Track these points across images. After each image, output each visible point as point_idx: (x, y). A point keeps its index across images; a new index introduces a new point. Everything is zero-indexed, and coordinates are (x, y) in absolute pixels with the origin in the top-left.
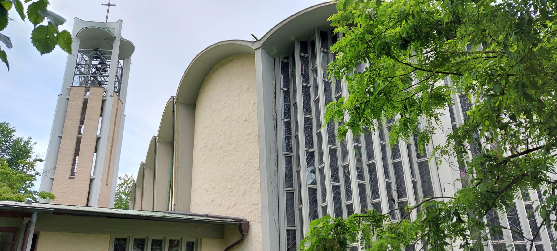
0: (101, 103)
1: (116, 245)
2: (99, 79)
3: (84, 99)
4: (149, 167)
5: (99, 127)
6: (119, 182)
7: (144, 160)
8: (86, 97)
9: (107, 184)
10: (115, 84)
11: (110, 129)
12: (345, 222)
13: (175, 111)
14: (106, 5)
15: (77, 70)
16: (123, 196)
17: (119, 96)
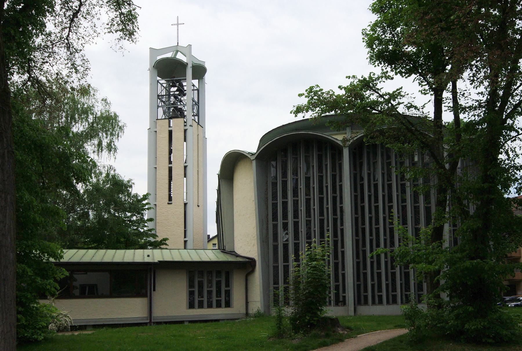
0: (183, 133)
3: (169, 131)
9: (198, 206)
10: (193, 109)
12: (475, 227)
14: (175, 25)
15: (159, 100)
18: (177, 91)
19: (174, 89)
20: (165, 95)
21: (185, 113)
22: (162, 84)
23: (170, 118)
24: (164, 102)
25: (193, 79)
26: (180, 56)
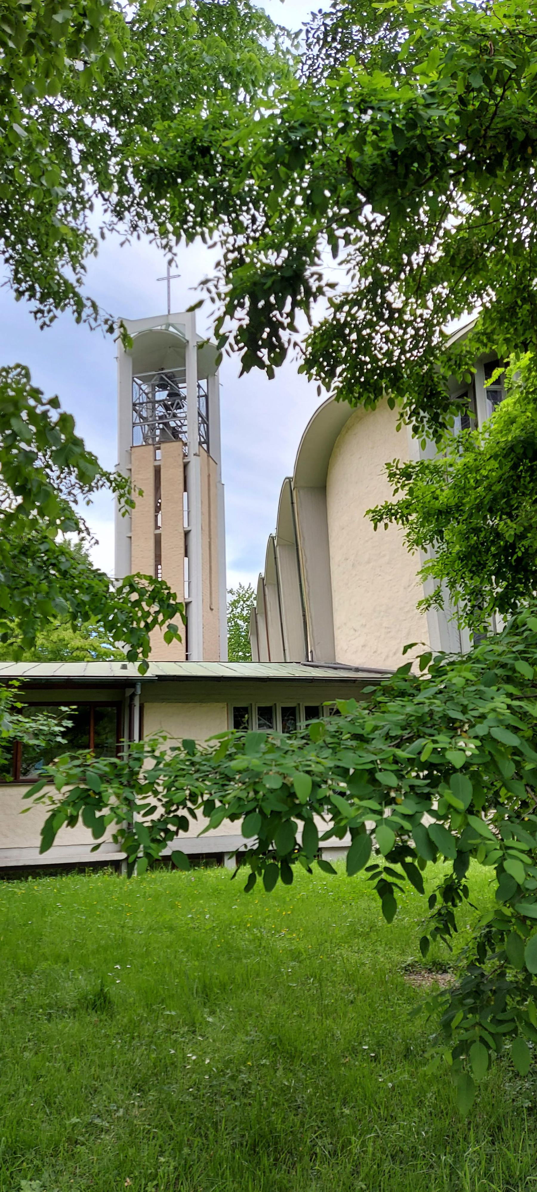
0: (181, 469)
1: (235, 716)
2: (172, 424)
3: (155, 467)
4: (269, 582)
5: (186, 514)
6: (230, 598)
7: (263, 571)
8: (157, 463)
11: (202, 514)
13: (295, 501)
14: (163, 279)
16: (240, 622)
17: (208, 451)
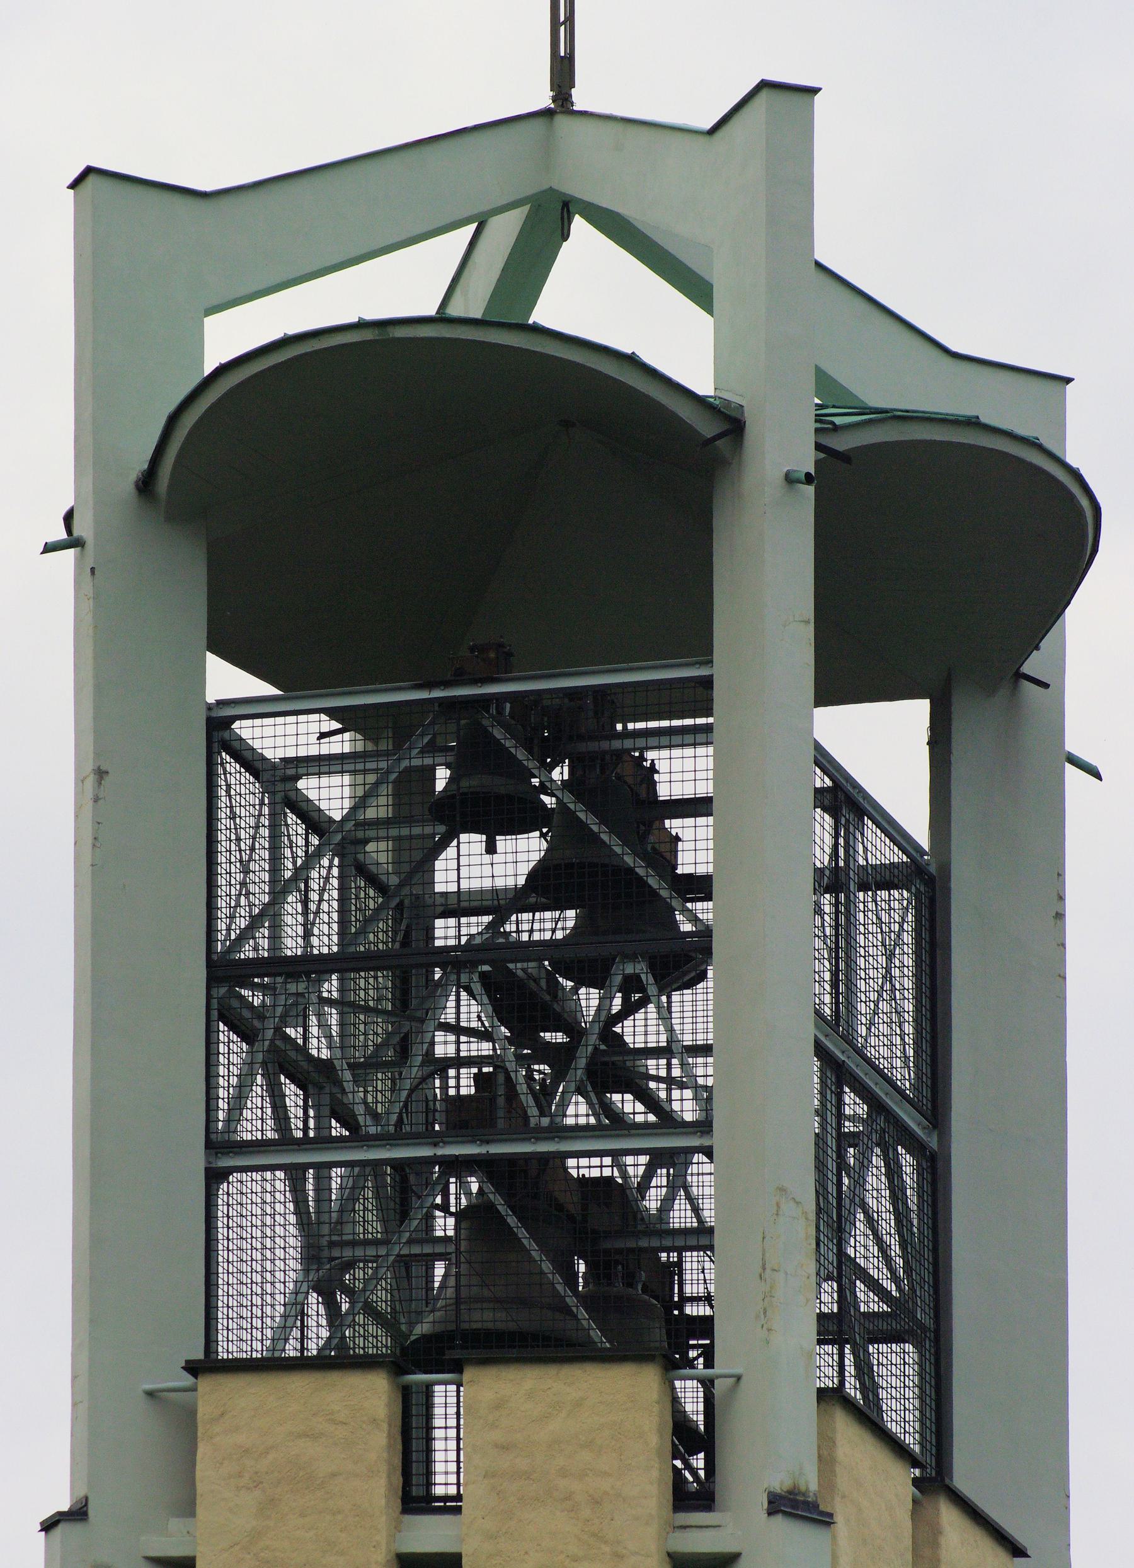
10: (834, 1217)
15: (232, 1051)
18: (542, 889)
19: (484, 863)
20: (342, 963)
21: (697, 1274)
22: (279, 780)
23: (425, 1355)
24: (315, 1077)
25: (833, 689)
26: (596, 297)
